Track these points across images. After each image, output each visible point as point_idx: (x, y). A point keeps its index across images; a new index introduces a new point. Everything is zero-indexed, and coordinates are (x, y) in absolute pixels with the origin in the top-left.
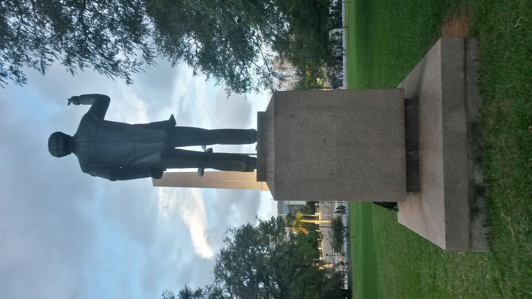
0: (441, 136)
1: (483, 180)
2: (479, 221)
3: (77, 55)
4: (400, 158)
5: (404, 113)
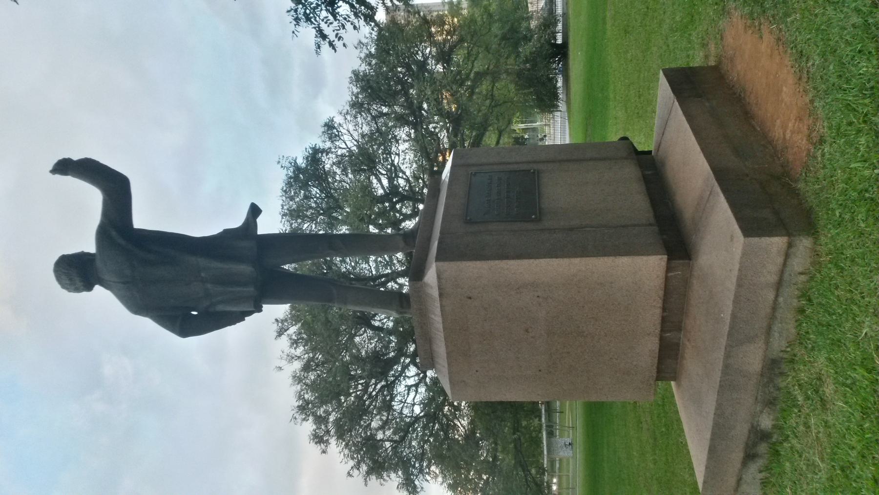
1: (773, 425)
2: (753, 468)
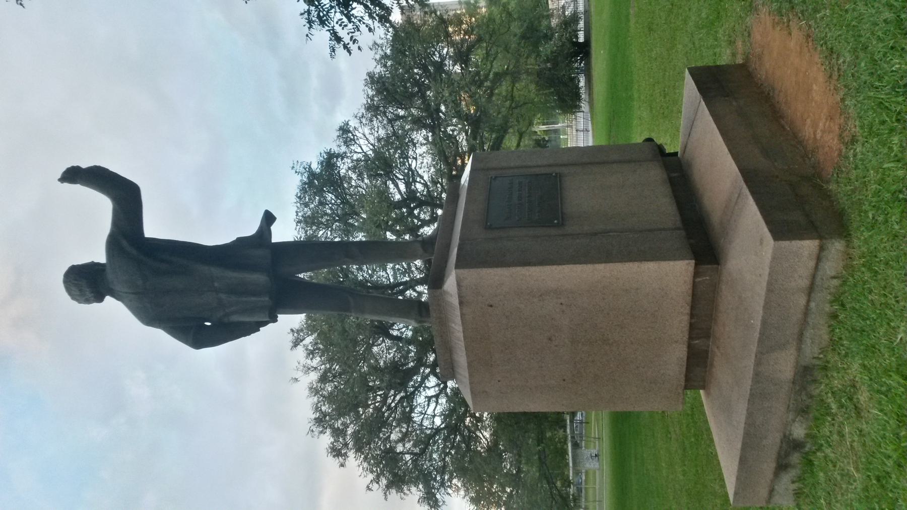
0: (750, 382)
4: (678, 359)
5: (690, 298)
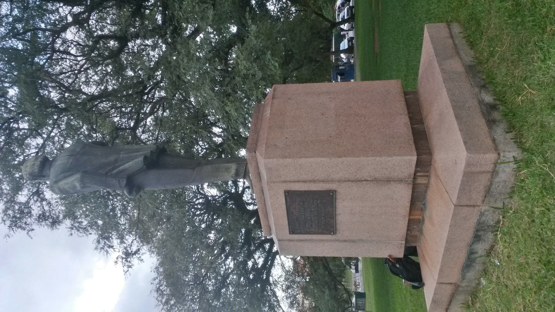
3: (45, 78)
